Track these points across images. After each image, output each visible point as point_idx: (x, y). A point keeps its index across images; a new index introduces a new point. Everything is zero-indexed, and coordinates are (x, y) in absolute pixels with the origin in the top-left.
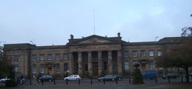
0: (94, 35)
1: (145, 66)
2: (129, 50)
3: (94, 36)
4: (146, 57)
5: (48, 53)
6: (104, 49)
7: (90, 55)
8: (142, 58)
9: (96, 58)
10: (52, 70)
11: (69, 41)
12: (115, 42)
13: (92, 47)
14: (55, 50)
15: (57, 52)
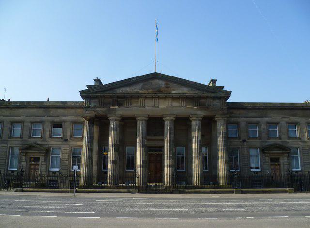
0: (156, 74)
1: (279, 161)
2: (240, 120)
3: (155, 76)
4: (280, 138)
5: (32, 119)
6: (156, 113)
7: (141, 126)
8: (271, 142)
9: (158, 138)
10: (40, 163)
11: (96, 83)
12: (212, 93)
13: (150, 103)
14: (52, 112)
15: (57, 116)
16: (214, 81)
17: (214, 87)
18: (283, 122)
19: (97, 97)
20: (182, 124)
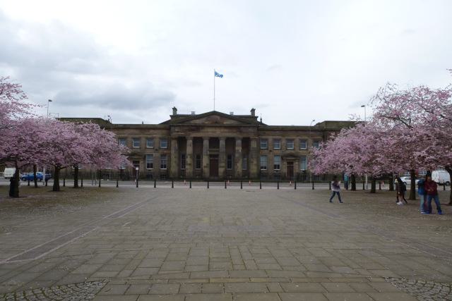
3: (214, 113)
4: (294, 149)
5: (132, 136)
6: (215, 135)
7: (206, 143)
8: (288, 152)
16: (253, 111)
17: (209, 166)
18: (297, 139)
19: (179, 126)
20: (230, 142)
